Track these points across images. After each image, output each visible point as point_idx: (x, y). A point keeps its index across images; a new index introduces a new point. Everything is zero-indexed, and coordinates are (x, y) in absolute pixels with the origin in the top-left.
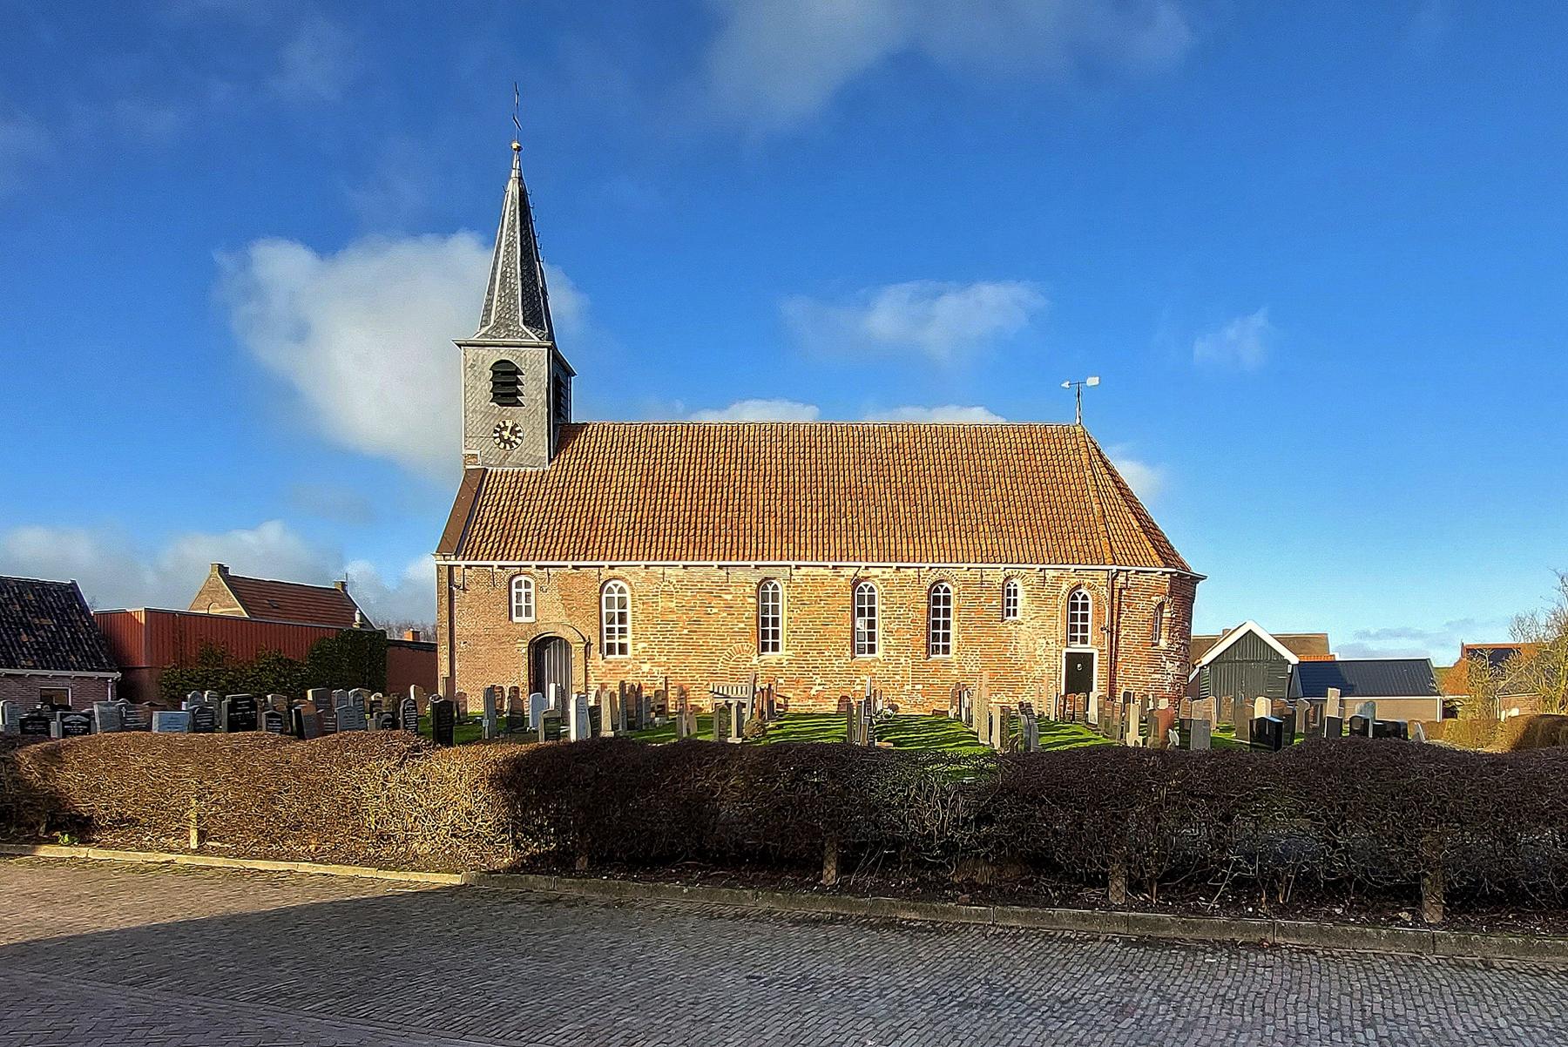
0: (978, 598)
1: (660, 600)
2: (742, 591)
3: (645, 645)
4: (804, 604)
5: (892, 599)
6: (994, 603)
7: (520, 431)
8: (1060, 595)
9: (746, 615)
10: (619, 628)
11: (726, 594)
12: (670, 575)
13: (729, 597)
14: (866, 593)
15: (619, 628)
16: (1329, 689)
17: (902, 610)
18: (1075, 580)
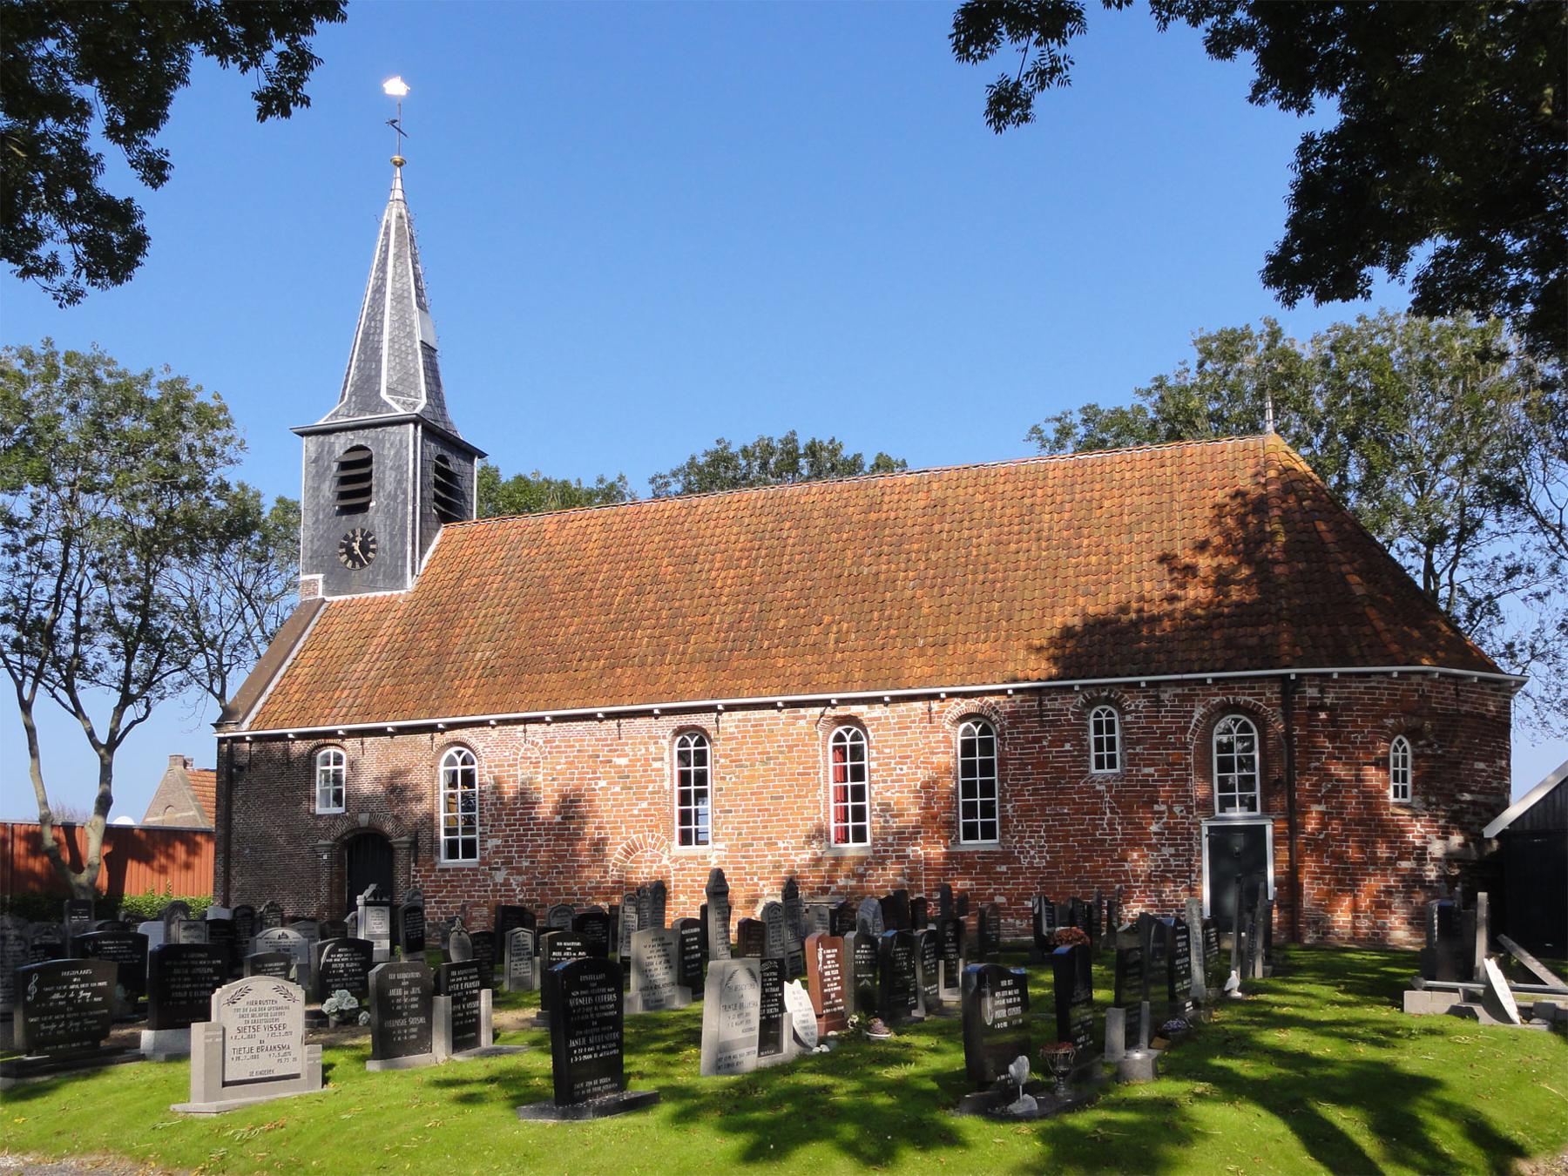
0: (1038, 740)
1: (519, 772)
2: (643, 751)
3: (499, 842)
4: (741, 766)
5: (887, 751)
6: (1068, 747)
7: (374, 551)
8: (1192, 726)
9: (650, 789)
10: (335, 764)
11: (618, 756)
12: (535, 733)
13: (623, 761)
14: (848, 743)
15: (335, 764)
16: (320, 577)
17: (905, 767)
18: (1218, 699)
